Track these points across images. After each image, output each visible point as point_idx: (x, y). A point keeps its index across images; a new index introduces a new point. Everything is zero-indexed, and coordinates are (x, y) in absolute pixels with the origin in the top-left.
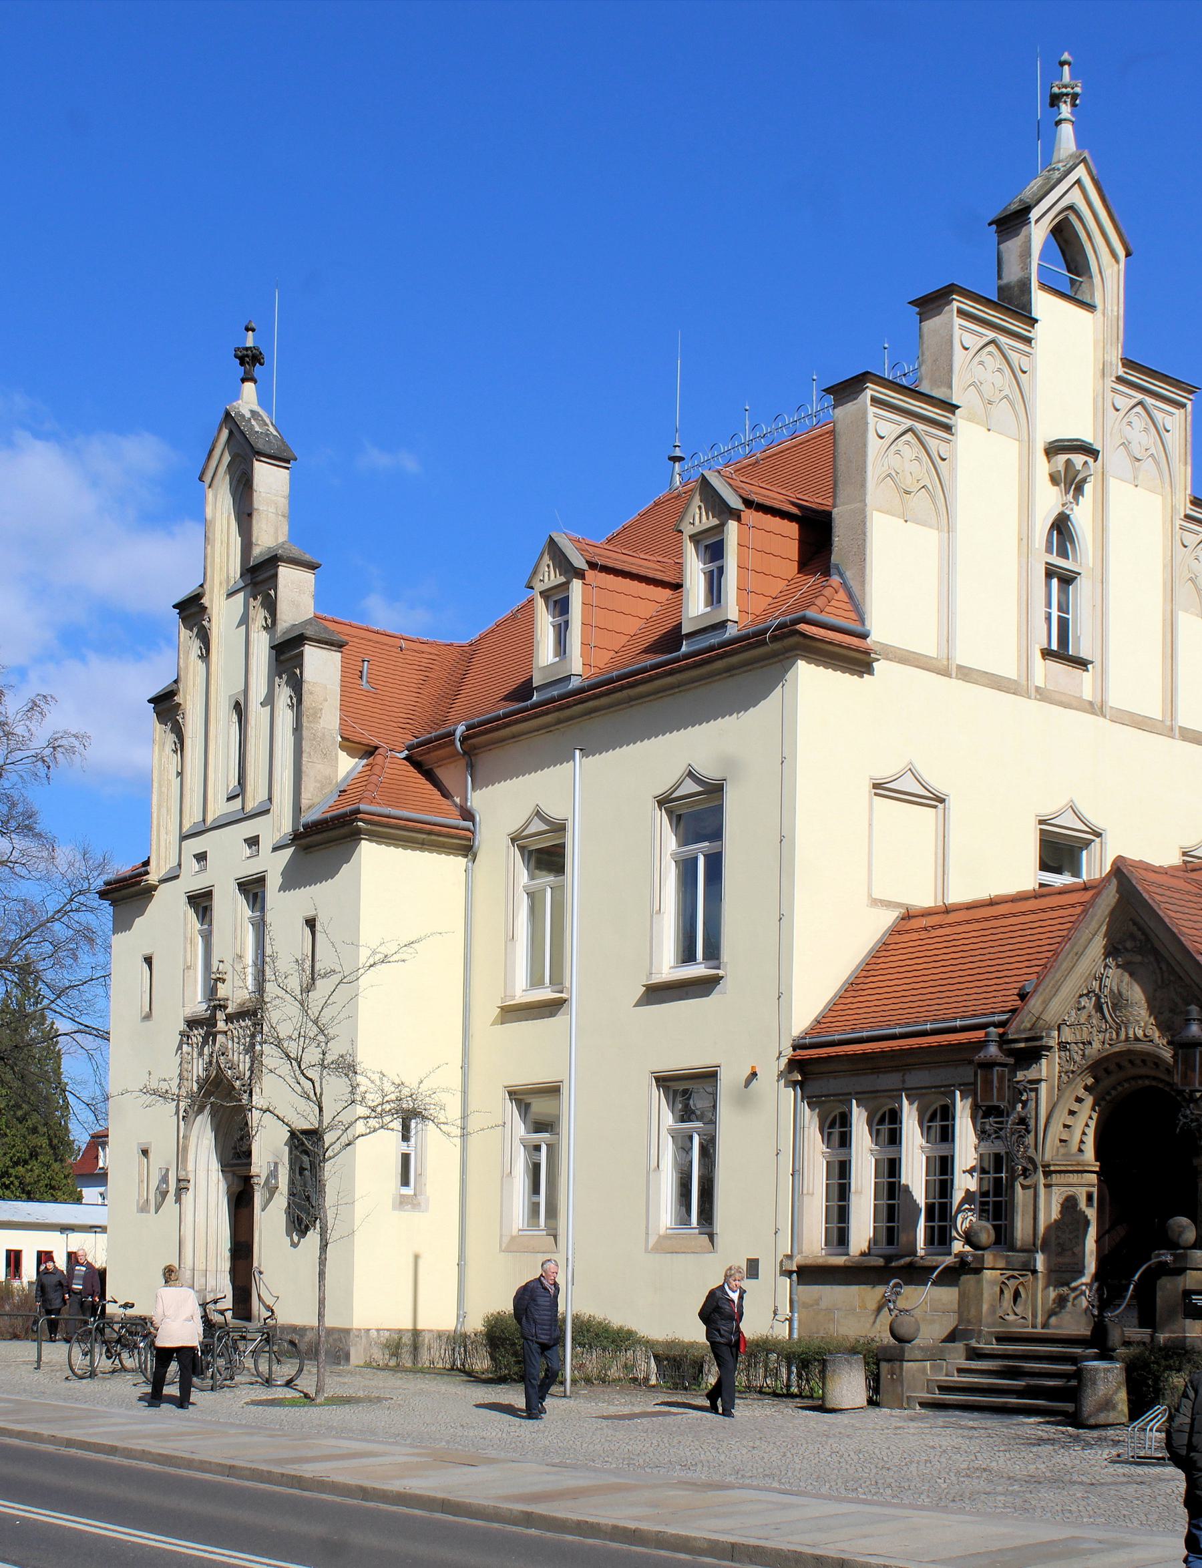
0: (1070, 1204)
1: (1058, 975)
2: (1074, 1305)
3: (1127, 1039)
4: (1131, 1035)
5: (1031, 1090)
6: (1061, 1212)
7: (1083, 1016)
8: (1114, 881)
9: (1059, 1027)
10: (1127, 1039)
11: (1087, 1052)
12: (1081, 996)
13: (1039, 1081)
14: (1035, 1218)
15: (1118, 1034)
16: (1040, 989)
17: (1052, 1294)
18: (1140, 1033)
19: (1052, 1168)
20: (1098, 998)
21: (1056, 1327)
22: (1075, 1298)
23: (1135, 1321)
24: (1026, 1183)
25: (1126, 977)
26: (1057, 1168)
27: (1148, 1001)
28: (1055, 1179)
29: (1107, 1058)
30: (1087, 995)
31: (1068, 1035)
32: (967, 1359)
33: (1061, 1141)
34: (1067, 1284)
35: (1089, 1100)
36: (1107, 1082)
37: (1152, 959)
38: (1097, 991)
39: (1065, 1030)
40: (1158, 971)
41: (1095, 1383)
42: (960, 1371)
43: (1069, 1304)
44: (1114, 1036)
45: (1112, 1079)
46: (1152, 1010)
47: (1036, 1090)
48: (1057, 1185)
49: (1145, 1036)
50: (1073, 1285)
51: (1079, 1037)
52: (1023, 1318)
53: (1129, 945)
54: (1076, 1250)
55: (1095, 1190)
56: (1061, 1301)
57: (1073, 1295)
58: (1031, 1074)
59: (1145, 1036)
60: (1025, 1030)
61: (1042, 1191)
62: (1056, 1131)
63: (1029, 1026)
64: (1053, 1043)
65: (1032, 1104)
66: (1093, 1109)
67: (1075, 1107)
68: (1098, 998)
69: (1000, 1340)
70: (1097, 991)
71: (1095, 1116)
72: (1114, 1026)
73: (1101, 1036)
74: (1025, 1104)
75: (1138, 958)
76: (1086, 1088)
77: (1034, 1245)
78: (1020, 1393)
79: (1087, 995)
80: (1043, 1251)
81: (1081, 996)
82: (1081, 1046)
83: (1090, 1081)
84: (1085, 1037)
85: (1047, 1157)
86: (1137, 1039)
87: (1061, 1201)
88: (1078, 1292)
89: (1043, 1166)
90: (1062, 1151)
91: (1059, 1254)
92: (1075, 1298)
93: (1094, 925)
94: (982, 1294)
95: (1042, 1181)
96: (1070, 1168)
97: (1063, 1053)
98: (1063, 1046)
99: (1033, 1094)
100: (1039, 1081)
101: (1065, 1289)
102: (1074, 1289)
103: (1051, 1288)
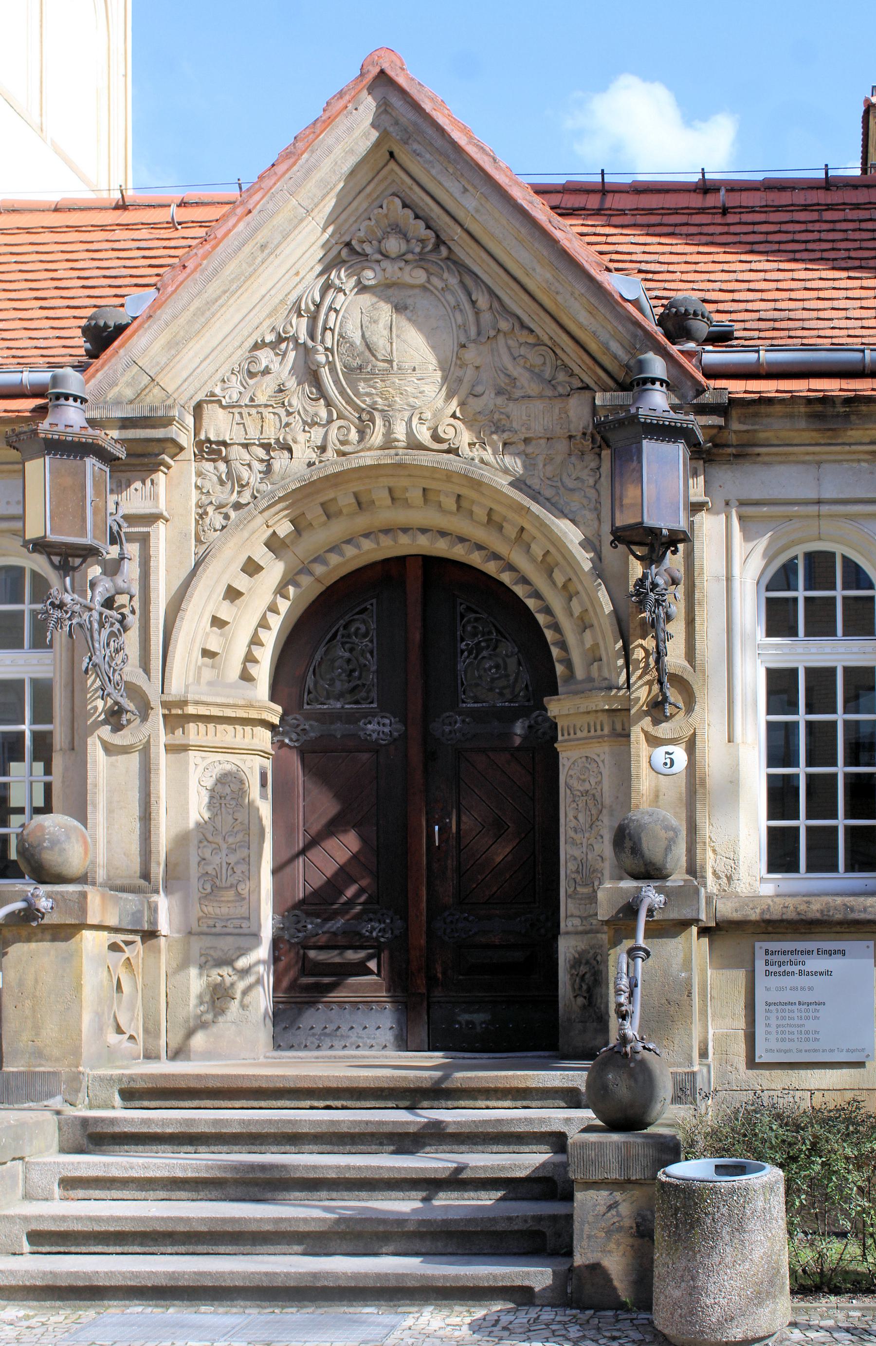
0: (227, 792)
1: (214, 289)
2: (243, 1006)
3: (388, 443)
4: (400, 432)
5: (131, 538)
6: (210, 806)
7: (264, 391)
8: (369, 105)
9: (198, 409)
10: (388, 443)
11: (276, 465)
12: (256, 347)
13: (152, 518)
14: (146, 817)
15: (362, 433)
16: (165, 314)
17: (196, 982)
18: (424, 435)
19: (191, 710)
20: (306, 352)
21: (208, 1055)
22: (245, 993)
23: (387, 1036)
24: (117, 739)
25: (385, 311)
26: (203, 711)
27: (444, 367)
28: (195, 733)
29: (335, 480)
30: (274, 345)
31: (219, 425)
32: (63, 1150)
33: (207, 653)
34: (229, 962)
35: (275, 569)
36: (320, 537)
37: (453, 281)
38: (303, 337)
39: (211, 412)
40: (467, 306)
41: (740, 1228)
42: (69, 1184)
43: (234, 1006)
44: (354, 436)
45: (337, 530)
46: (452, 384)
47: (144, 540)
48: (200, 748)
49: (436, 438)
50: (242, 963)
51: (253, 433)
52: (132, 1037)
53: (393, 245)
54: (243, 888)
55: (268, 764)
56: (218, 997)
57: (241, 985)
58: (134, 500)
59: (436, 438)
60: (118, 403)
61: (162, 760)
62: (193, 629)
63: (129, 393)
64: (185, 439)
65: (131, 570)
66: (281, 591)
67: (242, 582)
68: (306, 352)
69: (131, 1095)
70: (303, 337)
71: (284, 606)
72: (349, 411)
73: (317, 435)
74: (113, 568)
75: (420, 276)
76: (274, 544)
77: (146, 876)
78: (316, 1241)
79: (274, 345)
80: (168, 891)
81: (256, 347)
82: (261, 453)
83: (284, 528)
84: (271, 434)
85: (176, 687)
86: (415, 445)
87: (209, 783)
88: (251, 979)
89: (164, 704)
90: (208, 674)
91: (205, 897)
92: (245, 993)
93: (311, 187)
94: (78, 988)
95: (163, 738)
96: (229, 713)
97: (208, 466)
98: (211, 450)
99: (133, 549)
100: (152, 518)
101: (225, 971)
102: (245, 972)
103: (193, 972)
